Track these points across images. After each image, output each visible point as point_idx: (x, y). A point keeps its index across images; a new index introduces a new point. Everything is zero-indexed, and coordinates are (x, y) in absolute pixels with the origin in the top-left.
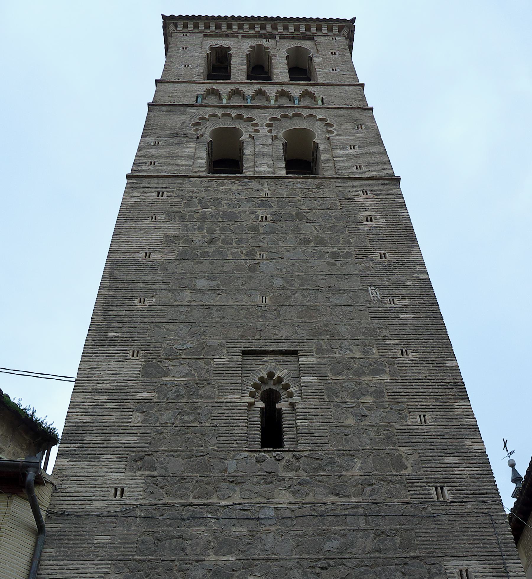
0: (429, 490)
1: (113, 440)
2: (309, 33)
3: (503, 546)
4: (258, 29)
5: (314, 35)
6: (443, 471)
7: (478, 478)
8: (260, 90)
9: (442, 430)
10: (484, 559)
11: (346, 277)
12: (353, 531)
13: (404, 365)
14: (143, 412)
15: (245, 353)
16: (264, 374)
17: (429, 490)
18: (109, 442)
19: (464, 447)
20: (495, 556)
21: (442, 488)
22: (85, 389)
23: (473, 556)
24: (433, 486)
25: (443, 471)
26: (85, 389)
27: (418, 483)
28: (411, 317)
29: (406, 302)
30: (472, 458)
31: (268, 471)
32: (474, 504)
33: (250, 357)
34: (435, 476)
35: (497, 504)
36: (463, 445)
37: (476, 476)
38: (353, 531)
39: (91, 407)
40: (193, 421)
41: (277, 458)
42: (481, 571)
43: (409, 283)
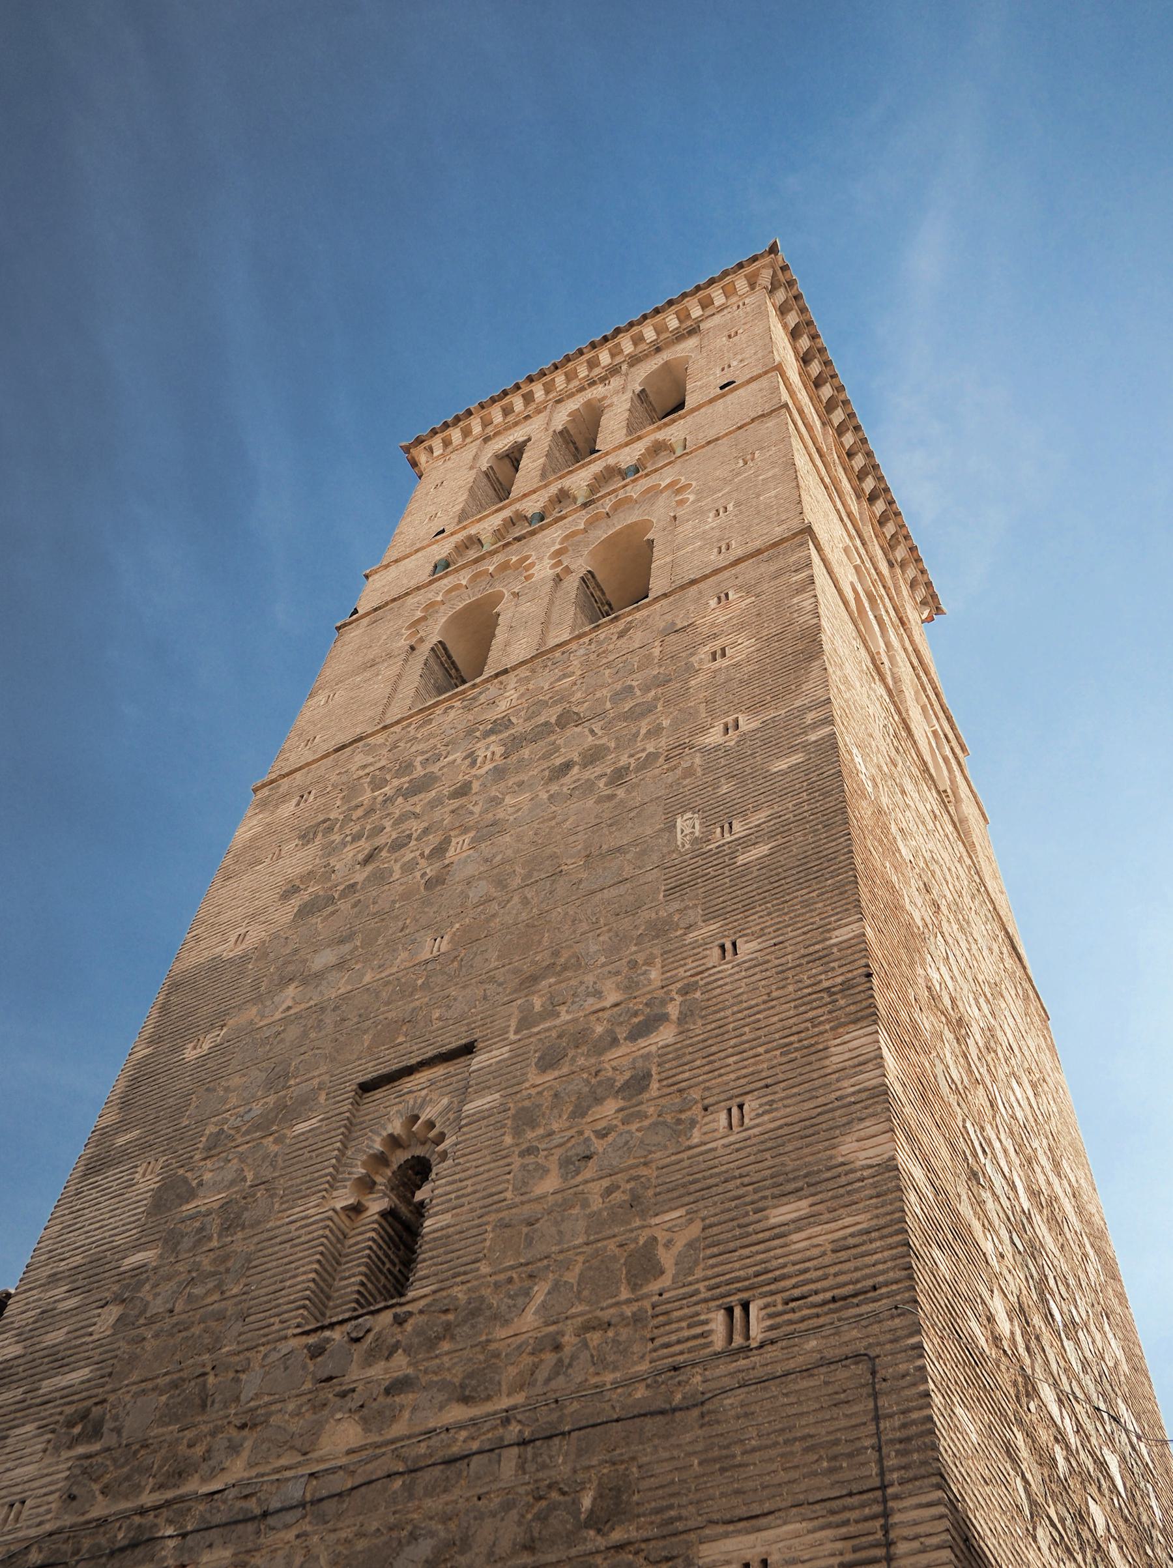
0: (706, 1322)
1: (46, 1386)
2: (689, 323)
3: (893, 1454)
4: (583, 372)
5: (699, 321)
6: (758, 1253)
7: (855, 1246)
8: (561, 490)
9: (781, 1132)
10: (824, 1513)
11: (632, 815)
12: (479, 1499)
13: (715, 985)
14: (124, 1301)
15: (366, 1087)
16: (396, 1127)
17: (706, 1322)
18: (788, 1249)
19: (834, 1162)
20: (861, 1493)
21: (745, 1307)
22: (36, 1280)
23: (757, 1516)
24: (719, 1307)
25: (758, 1253)
26: (36, 1280)
27: (681, 1308)
28: (764, 849)
29: (761, 816)
30: (849, 1188)
31: (325, 1376)
32: (828, 1332)
33: (378, 1094)
34: (733, 1275)
35: (899, 1315)
36: (831, 1158)
37: (851, 1241)
38: (479, 1499)
39: (31, 1320)
40: (208, 1293)
41: (354, 1335)
42: (806, 1557)
43: (782, 765)
